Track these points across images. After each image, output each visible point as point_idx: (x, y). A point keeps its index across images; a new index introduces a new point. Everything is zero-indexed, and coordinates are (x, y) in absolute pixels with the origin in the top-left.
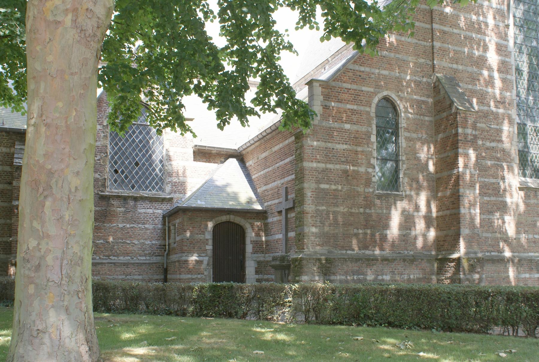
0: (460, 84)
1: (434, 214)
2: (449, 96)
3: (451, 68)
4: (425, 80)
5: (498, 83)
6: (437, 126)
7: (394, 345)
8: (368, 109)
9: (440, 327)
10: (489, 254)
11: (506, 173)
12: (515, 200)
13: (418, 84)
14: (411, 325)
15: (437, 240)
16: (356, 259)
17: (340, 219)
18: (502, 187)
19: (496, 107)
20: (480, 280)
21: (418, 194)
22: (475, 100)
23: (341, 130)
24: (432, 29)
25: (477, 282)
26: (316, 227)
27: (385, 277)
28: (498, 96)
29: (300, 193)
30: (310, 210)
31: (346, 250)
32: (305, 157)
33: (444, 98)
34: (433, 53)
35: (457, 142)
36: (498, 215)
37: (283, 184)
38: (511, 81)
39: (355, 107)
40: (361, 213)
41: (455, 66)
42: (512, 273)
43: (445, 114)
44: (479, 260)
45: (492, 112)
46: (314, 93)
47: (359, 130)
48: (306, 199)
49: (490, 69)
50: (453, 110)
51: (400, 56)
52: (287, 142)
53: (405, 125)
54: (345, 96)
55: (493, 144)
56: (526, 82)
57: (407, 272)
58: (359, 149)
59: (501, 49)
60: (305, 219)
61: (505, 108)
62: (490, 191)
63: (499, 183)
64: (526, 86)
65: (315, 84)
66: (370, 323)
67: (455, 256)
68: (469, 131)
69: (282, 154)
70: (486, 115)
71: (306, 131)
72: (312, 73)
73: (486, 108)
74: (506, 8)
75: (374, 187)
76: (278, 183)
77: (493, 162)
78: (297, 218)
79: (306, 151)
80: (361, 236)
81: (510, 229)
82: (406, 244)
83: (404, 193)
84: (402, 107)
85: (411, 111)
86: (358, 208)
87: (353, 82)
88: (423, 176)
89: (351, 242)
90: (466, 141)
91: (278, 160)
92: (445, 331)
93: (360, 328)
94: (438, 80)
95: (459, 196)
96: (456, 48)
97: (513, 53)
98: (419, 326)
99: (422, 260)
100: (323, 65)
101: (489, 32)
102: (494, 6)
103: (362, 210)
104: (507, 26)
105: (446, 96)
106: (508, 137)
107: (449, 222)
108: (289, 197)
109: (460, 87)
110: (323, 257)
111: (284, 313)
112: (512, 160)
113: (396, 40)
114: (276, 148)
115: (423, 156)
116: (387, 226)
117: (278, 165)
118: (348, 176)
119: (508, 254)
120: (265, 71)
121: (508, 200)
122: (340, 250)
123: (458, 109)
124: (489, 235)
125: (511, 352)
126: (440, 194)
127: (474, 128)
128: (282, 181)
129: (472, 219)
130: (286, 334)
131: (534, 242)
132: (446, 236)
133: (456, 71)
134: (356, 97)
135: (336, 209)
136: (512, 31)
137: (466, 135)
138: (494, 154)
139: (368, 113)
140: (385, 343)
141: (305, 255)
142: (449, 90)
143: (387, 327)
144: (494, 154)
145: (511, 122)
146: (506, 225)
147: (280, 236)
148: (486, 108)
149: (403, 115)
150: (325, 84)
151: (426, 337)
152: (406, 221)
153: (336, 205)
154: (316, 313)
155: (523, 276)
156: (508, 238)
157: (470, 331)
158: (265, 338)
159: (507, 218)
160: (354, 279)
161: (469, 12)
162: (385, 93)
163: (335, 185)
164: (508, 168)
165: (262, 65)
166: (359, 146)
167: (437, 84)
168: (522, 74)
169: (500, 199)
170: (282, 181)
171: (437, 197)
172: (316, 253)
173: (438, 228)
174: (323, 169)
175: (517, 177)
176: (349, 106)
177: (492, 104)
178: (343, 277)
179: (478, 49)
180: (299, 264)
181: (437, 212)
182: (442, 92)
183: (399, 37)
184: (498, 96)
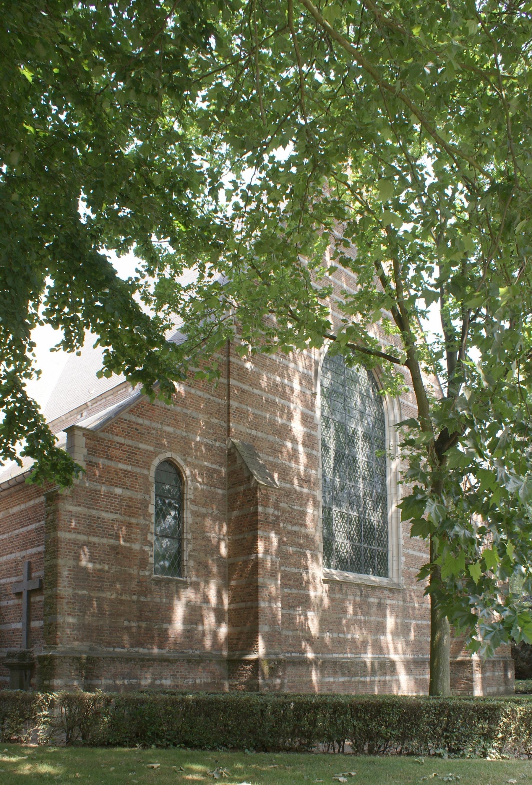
0: (260, 455)
1: (226, 607)
2: (247, 467)
3: (250, 434)
4: (217, 444)
5: (303, 459)
6: (231, 502)
7: (205, 774)
8: (145, 472)
9: (252, 746)
10: (289, 655)
11: (309, 562)
12: (319, 593)
13: (209, 448)
14: (215, 744)
15: (229, 637)
16: (128, 659)
17: (106, 607)
18: (305, 578)
19: (300, 486)
20: (282, 685)
21: (207, 582)
22: (276, 476)
23: (110, 495)
24: (229, 385)
25: (278, 687)
26: (74, 616)
27: (164, 682)
28: (302, 473)
29: (52, 572)
30: (67, 594)
31: (114, 647)
32: (60, 525)
33: (241, 468)
34: (229, 413)
35: (256, 522)
36: (299, 610)
37: (24, 557)
38: (316, 458)
39: (129, 468)
40: (134, 602)
41: (254, 432)
42: (314, 677)
43: (242, 488)
44: (280, 662)
45: (296, 490)
46: (76, 444)
47: (134, 497)
48: (60, 580)
49: (294, 441)
50: (252, 484)
51: (189, 412)
52: (32, 503)
53: (192, 497)
54: (117, 453)
55: (296, 528)
56: (332, 460)
57: (192, 675)
58: (134, 521)
59: (307, 420)
60: (59, 606)
61: (309, 488)
62: (291, 583)
63: (301, 574)
64: (332, 466)
65: (76, 432)
66: (159, 742)
67: (253, 657)
68: (271, 511)
69: (25, 518)
70: (288, 494)
71: (64, 491)
72: (64, 418)
73: (288, 486)
74: (313, 374)
75: (150, 570)
76: (17, 555)
77: (295, 549)
78: (46, 604)
79: (62, 517)
80: (134, 630)
81: (313, 626)
82: (191, 641)
83: (188, 579)
84: (188, 472)
85: (200, 480)
86: (131, 595)
87: (128, 436)
88: (213, 560)
89: (121, 637)
90: (267, 522)
91: (18, 526)
92: (258, 751)
93: (149, 752)
94: (234, 445)
95: (257, 586)
96: (256, 411)
97: (319, 426)
98: (226, 746)
99: (210, 661)
100: (80, 410)
101: (294, 398)
102: (301, 369)
103: (135, 598)
104: (314, 395)
105: (244, 467)
106: (313, 520)
107: (245, 616)
108: (33, 575)
109: (259, 457)
110: (84, 656)
111: (37, 730)
112: (317, 548)
113: (185, 391)
114: (15, 510)
115: (213, 536)
116: (169, 620)
117: (17, 532)
118: (118, 553)
119: (310, 655)
120: (13, 405)
121: (312, 593)
122: (106, 647)
123: (258, 483)
124: (290, 633)
125: (350, 775)
126: (233, 583)
127: (276, 507)
128: (23, 553)
129: (274, 616)
130: (52, 764)
131: (339, 642)
132: (241, 633)
133: (255, 438)
134: (131, 455)
135: (100, 595)
136: (319, 401)
137: (267, 515)
138: (296, 540)
139: (146, 477)
140: (190, 771)
141: (58, 652)
142: (248, 460)
143: (184, 748)
144: (296, 540)
145: (316, 505)
146: (309, 622)
147: (19, 626)
148: (288, 486)
149: (189, 482)
150: (88, 433)
151: (242, 762)
152: (190, 615)
153: (101, 589)
154: (78, 731)
155: (327, 680)
156: (311, 636)
157: (290, 750)
158: (19, 772)
159: (310, 614)
160: (124, 684)
161: (274, 372)
162: (168, 455)
163: (100, 563)
164: (312, 557)
165: (9, 397)
166: (133, 517)
167: (232, 451)
168: (328, 452)
169: (303, 592)
170: (23, 553)
171: (229, 586)
172: (73, 649)
173: (232, 624)
174: (85, 542)
175: (322, 568)
176: (121, 466)
177: (296, 481)
178: (111, 682)
179: (281, 417)
180: (49, 663)
181: (229, 604)
182: (239, 461)
183: (188, 389)
184: (302, 473)
